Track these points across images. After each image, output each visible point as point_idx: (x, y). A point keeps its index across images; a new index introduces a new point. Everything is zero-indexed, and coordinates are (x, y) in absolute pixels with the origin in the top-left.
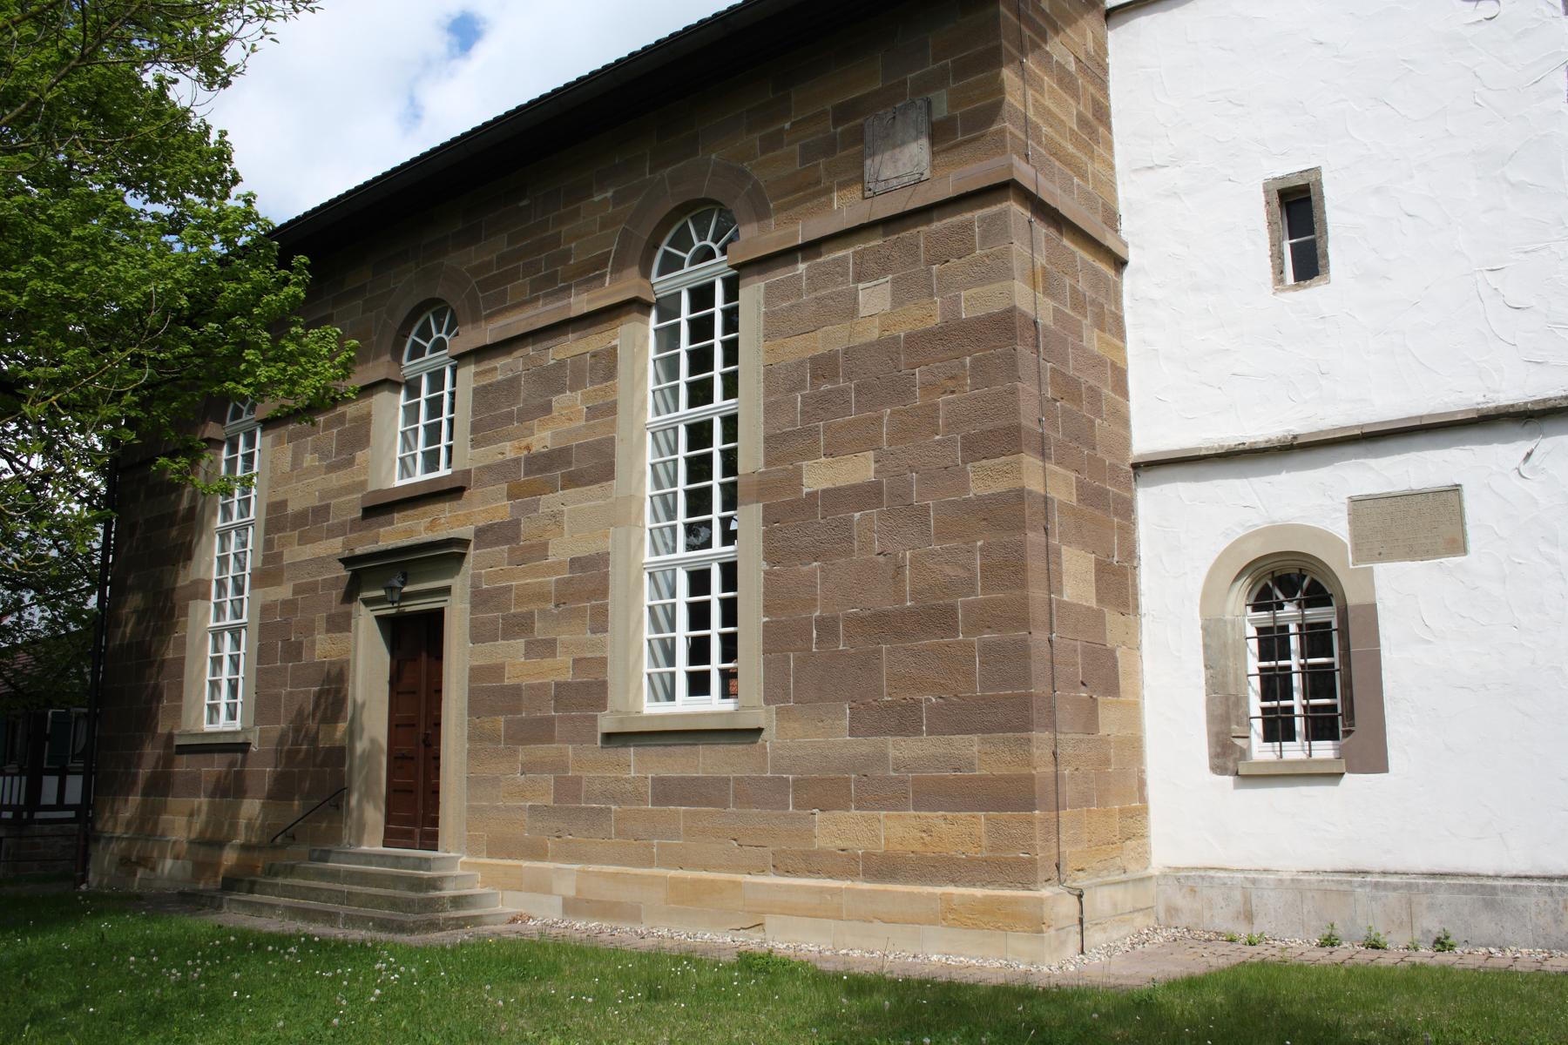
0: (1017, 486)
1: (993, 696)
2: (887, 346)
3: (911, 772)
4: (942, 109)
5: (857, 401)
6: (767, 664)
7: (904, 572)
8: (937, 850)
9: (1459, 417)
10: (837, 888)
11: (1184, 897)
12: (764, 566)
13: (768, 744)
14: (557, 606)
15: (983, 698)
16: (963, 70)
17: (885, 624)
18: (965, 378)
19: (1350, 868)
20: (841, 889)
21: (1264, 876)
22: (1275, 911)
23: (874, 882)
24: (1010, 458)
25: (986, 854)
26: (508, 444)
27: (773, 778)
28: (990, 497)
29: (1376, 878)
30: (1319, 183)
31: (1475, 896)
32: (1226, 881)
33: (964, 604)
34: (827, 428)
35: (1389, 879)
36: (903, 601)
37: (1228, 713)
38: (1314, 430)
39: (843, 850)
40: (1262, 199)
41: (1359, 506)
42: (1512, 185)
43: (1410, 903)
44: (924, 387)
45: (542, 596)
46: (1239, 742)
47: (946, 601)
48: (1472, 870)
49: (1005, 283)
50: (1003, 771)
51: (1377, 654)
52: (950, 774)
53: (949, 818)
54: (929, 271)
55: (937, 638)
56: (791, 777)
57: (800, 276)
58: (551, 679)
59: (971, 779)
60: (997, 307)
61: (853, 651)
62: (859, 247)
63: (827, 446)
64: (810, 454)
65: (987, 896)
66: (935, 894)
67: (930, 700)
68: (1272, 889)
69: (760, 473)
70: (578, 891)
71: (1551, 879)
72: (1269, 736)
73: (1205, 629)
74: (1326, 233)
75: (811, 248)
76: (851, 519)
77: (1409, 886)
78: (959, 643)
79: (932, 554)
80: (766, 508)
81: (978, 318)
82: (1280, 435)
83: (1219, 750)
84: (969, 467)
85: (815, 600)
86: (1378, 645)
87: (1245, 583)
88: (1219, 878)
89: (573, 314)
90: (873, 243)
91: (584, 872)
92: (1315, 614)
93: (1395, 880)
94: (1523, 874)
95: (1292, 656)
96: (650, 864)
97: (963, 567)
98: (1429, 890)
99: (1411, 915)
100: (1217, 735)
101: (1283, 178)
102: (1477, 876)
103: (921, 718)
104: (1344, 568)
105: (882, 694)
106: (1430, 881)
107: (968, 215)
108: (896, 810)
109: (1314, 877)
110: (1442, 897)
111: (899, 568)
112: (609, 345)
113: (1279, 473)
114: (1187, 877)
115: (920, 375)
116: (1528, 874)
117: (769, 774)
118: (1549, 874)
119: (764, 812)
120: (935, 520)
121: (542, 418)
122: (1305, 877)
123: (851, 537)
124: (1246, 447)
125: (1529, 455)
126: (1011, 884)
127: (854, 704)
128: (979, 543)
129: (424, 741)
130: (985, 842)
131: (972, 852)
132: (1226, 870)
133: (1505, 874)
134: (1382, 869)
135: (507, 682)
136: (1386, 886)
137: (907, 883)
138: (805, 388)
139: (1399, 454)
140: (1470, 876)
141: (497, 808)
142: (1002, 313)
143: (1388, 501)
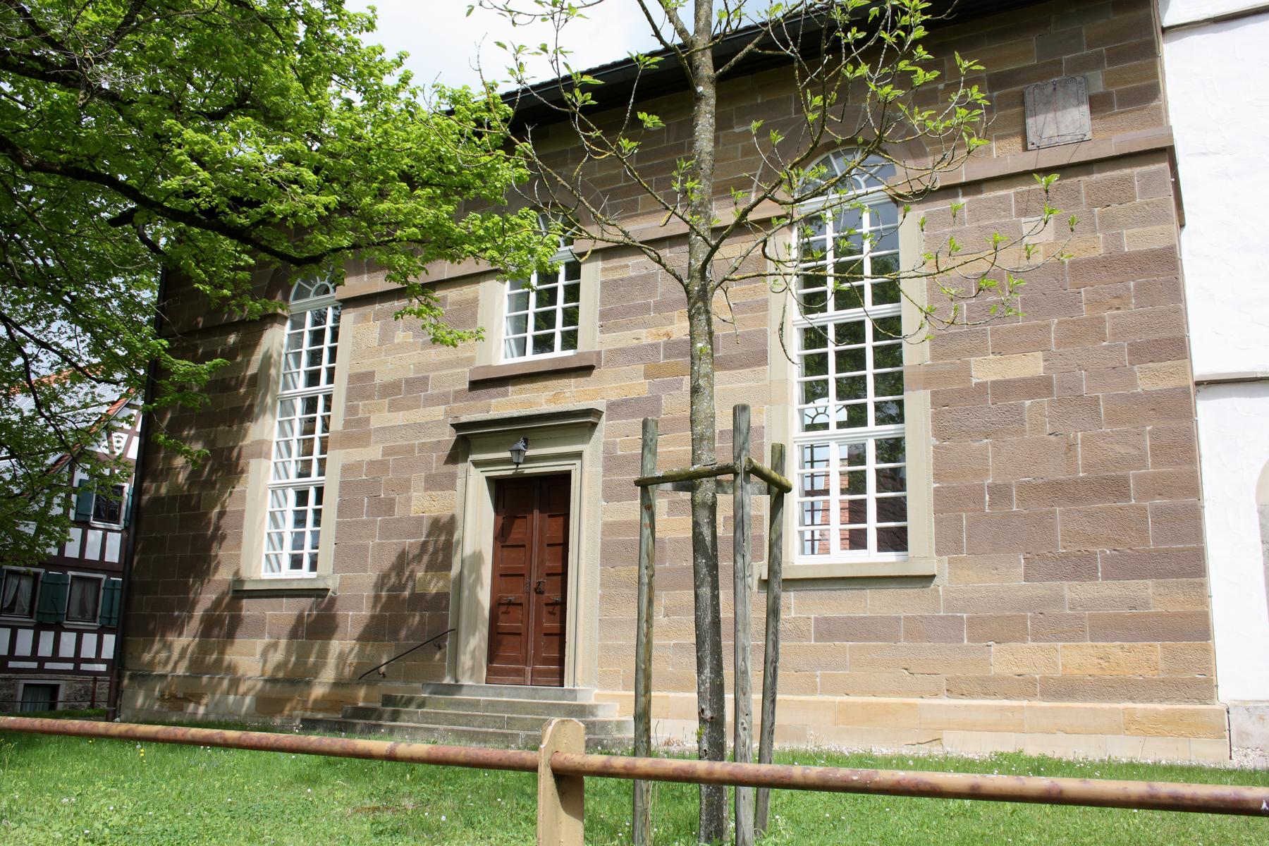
0: (1184, 384)
4: (1099, 86)
6: (938, 522)
7: (1075, 450)
8: (1116, 673)
12: (934, 441)
15: (1156, 551)
16: (1116, 57)
18: (1129, 298)
23: (1052, 701)
24: (1176, 362)
28: (1157, 392)
33: (1135, 476)
36: (1076, 472)
44: (1090, 302)
47: (1119, 473)
49: (1165, 226)
52: (1126, 612)
59: (1148, 615)
66: (1118, 709)
73: (1261, 513)
75: (972, 187)
76: (1022, 406)
78: (1132, 506)
79: (1104, 436)
80: (934, 394)
81: (1140, 252)
85: (987, 470)
97: (1134, 447)
111: (1071, 447)
117: (942, 614)
119: (937, 645)
123: (1022, 421)
126: (1188, 700)
127: (1029, 556)
128: (1148, 428)
131: (1149, 674)
142: (1164, 249)
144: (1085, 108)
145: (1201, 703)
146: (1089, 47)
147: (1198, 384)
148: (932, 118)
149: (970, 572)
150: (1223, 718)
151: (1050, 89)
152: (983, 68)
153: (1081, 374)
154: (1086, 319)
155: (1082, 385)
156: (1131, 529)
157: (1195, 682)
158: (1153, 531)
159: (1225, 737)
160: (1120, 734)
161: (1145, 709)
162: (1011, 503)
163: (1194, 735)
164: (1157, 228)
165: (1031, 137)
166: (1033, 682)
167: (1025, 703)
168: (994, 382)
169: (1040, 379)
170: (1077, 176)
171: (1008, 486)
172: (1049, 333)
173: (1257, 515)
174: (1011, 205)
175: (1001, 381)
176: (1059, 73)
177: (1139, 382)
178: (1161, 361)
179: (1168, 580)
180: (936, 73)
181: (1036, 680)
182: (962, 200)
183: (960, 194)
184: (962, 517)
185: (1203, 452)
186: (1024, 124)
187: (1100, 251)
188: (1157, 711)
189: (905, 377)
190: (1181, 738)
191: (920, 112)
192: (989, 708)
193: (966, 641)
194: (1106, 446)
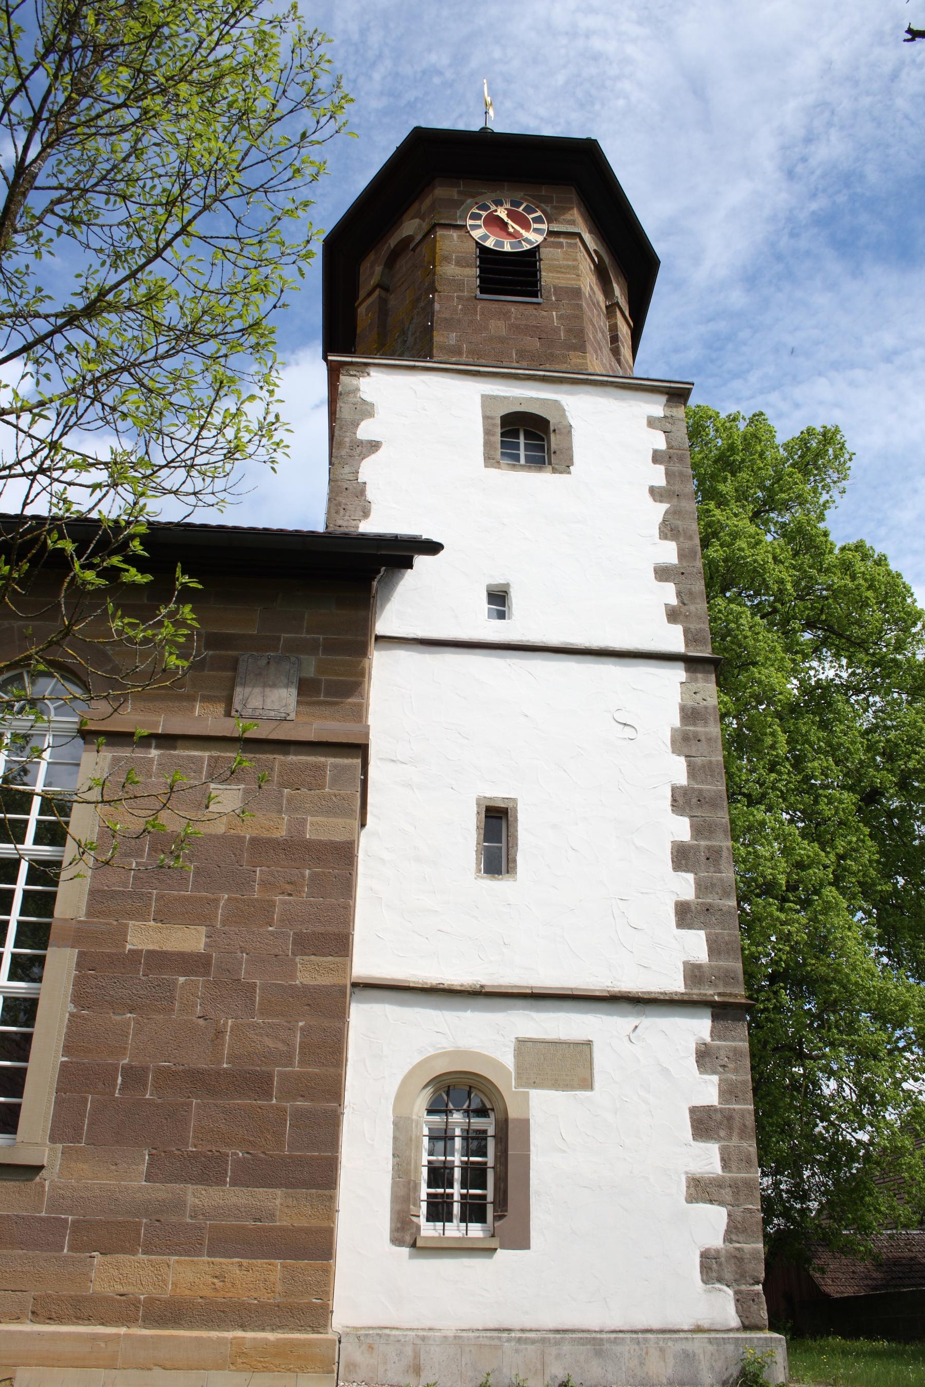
0: (341, 983)
1: (300, 1156)
2: (230, 842)
3: (210, 1220)
4: (310, 671)
5: (195, 881)
6: (59, 1103)
7: (223, 1039)
8: (230, 1295)
9: (597, 994)
10: (115, 1334)
11: (363, 1353)
12: (71, 1008)
13: (47, 1183)
15: (290, 1157)
16: (331, 648)
18: (303, 886)
20: (118, 1336)
21: (431, 1333)
22: (439, 1364)
23: (154, 1327)
24: (338, 959)
25: (279, 1300)
27: (48, 1219)
28: (314, 987)
29: (519, 1335)
30: (515, 809)
31: (589, 1347)
32: (400, 1338)
33: (280, 1073)
34: (160, 898)
36: (221, 1062)
37: (409, 1195)
38: (496, 984)
39: (121, 1295)
40: (475, 809)
41: (523, 1045)
42: (637, 848)
43: (543, 1353)
44: (264, 883)
46: (414, 1219)
47: (263, 1068)
48: (584, 1327)
49: (348, 821)
50: (304, 1223)
51: (527, 1157)
52: (250, 1223)
53: (245, 1264)
54: (281, 792)
55: (250, 1099)
56: (70, 1218)
57: (151, 760)
59: (272, 1229)
60: (339, 837)
61: (160, 1101)
62: (215, 753)
63: (157, 912)
64: (140, 915)
65: (281, 1339)
66: (226, 1338)
67: (236, 1154)
68: (437, 1345)
71: (635, 1332)
72: (433, 1216)
73: (396, 1124)
74: (517, 845)
75: (167, 740)
76: (175, 982)
77: (543, 1340)
78: (272, 1106)
79: (254, 1026)
80: (80, 954)
81: (320, 841)
82: (470, 982)
83: (399, 1225)
85: (125, 1048)
86: (529, 1150)
87: (429, 1091)
88: (395, 1335)
90: (228, 754)
92: (478, 1123)
94: (618, 1329)
95: (456, 1154)
97: (283, 1041)
98: (557, 1343)
99: (543, 1364)
100: (399, 1212)
101: (490, 799)
102: (588, 1331)
103: (226, 1171)
104: (508, 1087)
105: (188, 1143)
106: (558, 1336)
107: (322, 759)
108: (189, 1256)
109: (471, 1334)
110: (566, 1348)
111: (219, 1033)
113: (466, 1010)
114: (367, 1335)
115: (261, 874)
116: (622, 1329)
117: (43, 1214)
118: (634, 1328)
119: (31, 1253)
120: (261, 997)
122: (464, 1334)
123: (172, 998)
124: (445, 986)
125: (636, 1027)
126: (300, 1328)
127: (154, 1151)
128: (301, 1024)
129: (668, 1070)
130: (279, 1288)
131: (265, 1298)
132: (397, 1329)
133: (607, 1329)
134: (521, 1327)
136: (526, 1341)
137: (191, 1328)
139: (553, 1012)
140: (583, 1331)
142: (343, 843)
143: (543, 1045)
144: (294, 691)
145: (314, 1332)
146: (308, 632)
147: (355, 985)
148: (133, 626)
149: (85, 1166)
150: (334, 1349)
151: (263, 662)
152: (200, 587)
153: (242, 958)
154: (257, 900)
155: (241, 969)
156: (268, 1130)
157: (311, 1307)
158: (290, 1136)
159: (333, 1372)
160: (224, 1369)
161: (255, 1339)
162: (145, 1089)
163: (302, 1369)
164: (340, 821)
165: (237, 705)
166: (136, 1303)
167: (123, 1330)
168: (148, 951)
169: (199, 955)
170: (272, 753)
171: (145, 1070)
172: (217, 908)
173: (392, 1126)
174: (203, 767)
175: (157, 952)
176: (276, 649)
177: (298, 974)
178: (324, 955)
179: (298, 1190)
180: (148, 578)
181: (139, 1302)
182: (154, 753)
183: (154, 745)
184: (87, 1100)
185: (349, 1056)
186: (232, 689)
187: (281, 833)
188: (266, 1341)
189: (52, 931)
190: (289, 1374)
191: (122, 617)
192: (78, 1336)
193: (65, 1251)
194: (255, 1037)
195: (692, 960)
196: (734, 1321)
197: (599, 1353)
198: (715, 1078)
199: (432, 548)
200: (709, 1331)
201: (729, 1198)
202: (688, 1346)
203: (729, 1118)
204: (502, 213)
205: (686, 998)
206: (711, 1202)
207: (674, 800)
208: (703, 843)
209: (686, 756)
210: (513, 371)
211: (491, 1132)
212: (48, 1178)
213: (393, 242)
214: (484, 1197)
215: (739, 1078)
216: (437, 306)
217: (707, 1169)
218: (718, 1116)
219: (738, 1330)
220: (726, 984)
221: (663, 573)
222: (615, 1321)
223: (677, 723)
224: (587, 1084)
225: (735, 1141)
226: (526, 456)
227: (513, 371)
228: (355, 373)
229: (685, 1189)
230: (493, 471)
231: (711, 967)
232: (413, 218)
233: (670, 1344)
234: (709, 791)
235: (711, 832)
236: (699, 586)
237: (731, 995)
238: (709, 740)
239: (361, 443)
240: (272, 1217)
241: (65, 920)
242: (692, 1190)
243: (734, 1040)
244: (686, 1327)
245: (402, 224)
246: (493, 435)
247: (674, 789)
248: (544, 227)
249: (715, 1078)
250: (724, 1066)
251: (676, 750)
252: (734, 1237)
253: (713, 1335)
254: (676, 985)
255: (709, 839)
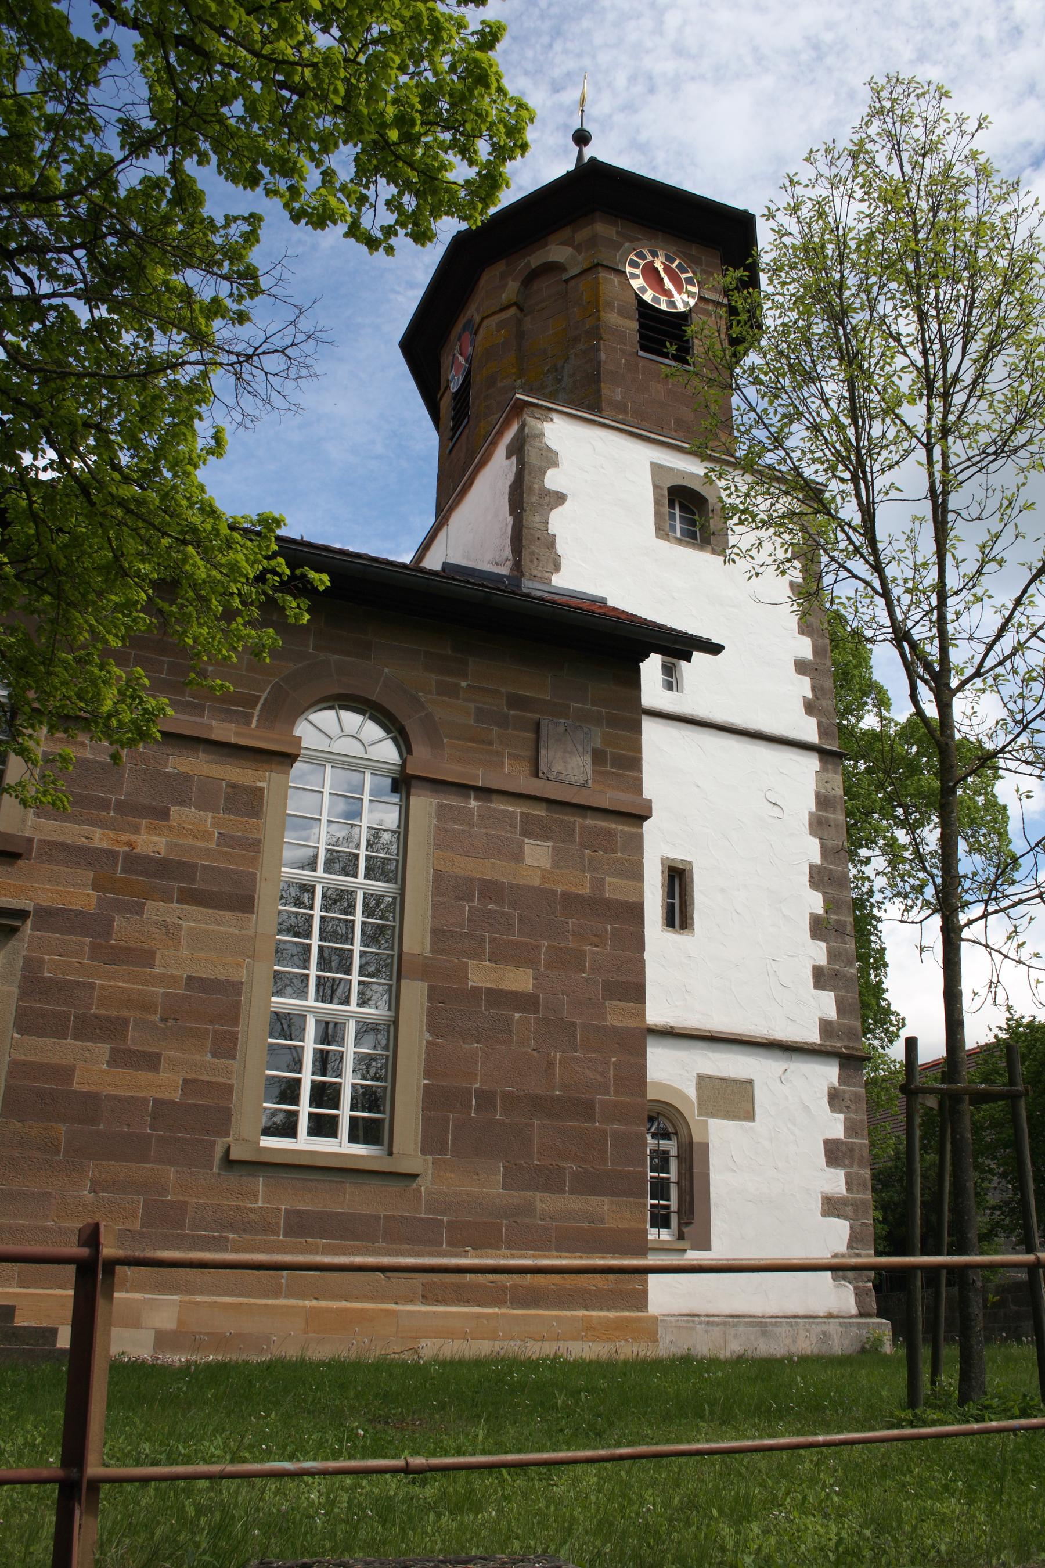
4: (598, 744)
6: (426, 1120)
9: (759, 1040)
12: (427, 1036)
13: (423, 1189)
14: (164, 1020)
17: (540, 1105)
19: (688, 1312)
26: (98, 830)
34: (493, 940)
35: (711, 1319)
41: (702, 1080)
43: (725, 1334)
45: (147, 1006)
48: (751, 1313)
54: (582, 852)
57: (472, 810)
58: (150, 1094)
69: (426, 957)
70: (180, 1322)
75: (485, 793)
76: (511, 1018)
77: (725, 1323)
78: (596, 1128)
84: (607, 1003)
85: (476, 1074)
86: (709, 1169)
89: (214, 737)
91: (190, 1302)
92: (664, 1144)
93: (716, 1319)
96: (277, 1295)
97: (601, 1075)
102: (754, 1316)
104: (692, 1115)
107: (614, 826)
110: (741, 1329)
111: (551, 1064)
112: (253, 784)
117: (423, 1215)
121: (154, 822)
126: (628, 1308)
128: (613, 1059)
135: (75, 1087)
137: (548, 1308)
138: (473, 901)
140: (751, 1316)
141: (45, 1229)
144: (588, 759)
149: (453, 1175)
154: (571, 949)
165: (543, 767)
167: (496, 1310)
168: (487, 989)
169: (529, 995)
172: (540, 953)
187: (586, 891)
195: (826, 1017)
196: (854, 1310)
197: (764, 1333)
198: (841, 1117)
199: (714, 649)
200: (838, 1317)
201: (851, 1214)
202: (825, 1328)
203: (851, 1149)
204: (658, 265)
205: (823, 1048)
206: (839, 1216)
207: (811, 877)
208: (832, 917)
209: (820, 839)
210: (679, 443)
211: (673, 1152)
212: (425, 1185)
213: (535, 260)
214: (667, 1207)
215: (859, 1118)
216: (603, 356)
217: (837, 1190)
218: (844, 1148)
219: (856, 1316)
220: (850, 1039)
221: (801, 667)
222: (772, 1309)
223: (813, 808)
224: (750, 1116)
225: (855, 1169)
226: (681, 528)
227: (679, 443)
228: (539, 416)
229: (820, 1205)
230: (663, 543)
231: (839, 1024)
232: (563, 243)
233: (813, 1326)
234: (836, 871)
235: (838, 908)
236: (829, 684)
237: (852, 1048)
238: (837, 826)
239: (548, 493)
240: (602, 1220)
241: (413, 955)
242: (826, 1207)
243: (855, 1086)
244: (822, 1314)
245: (546, 245)
246: (663, 506)
247: (812, 867)
248: (695, 290)
249: (841, 1117)
250: (848, 1107)
251: (813, 832)
252: (855, 1245)
253: (841, 1320)
254: (813, 1036)
255: (837, 914)
